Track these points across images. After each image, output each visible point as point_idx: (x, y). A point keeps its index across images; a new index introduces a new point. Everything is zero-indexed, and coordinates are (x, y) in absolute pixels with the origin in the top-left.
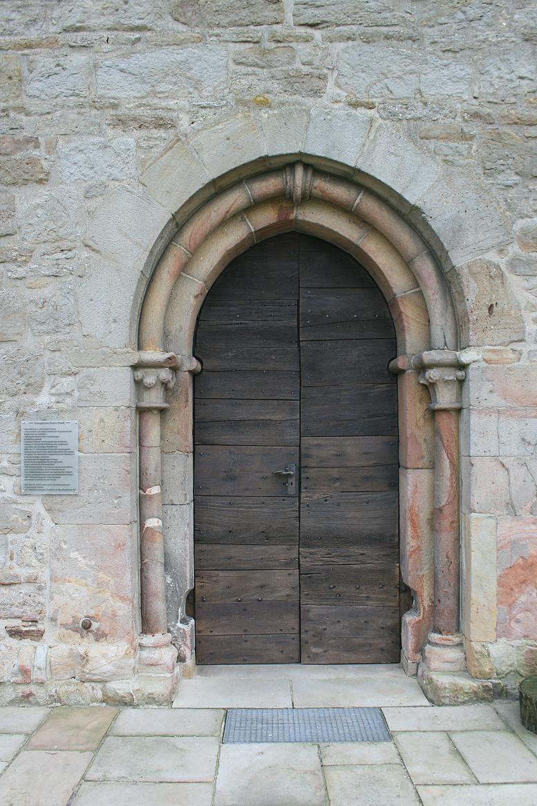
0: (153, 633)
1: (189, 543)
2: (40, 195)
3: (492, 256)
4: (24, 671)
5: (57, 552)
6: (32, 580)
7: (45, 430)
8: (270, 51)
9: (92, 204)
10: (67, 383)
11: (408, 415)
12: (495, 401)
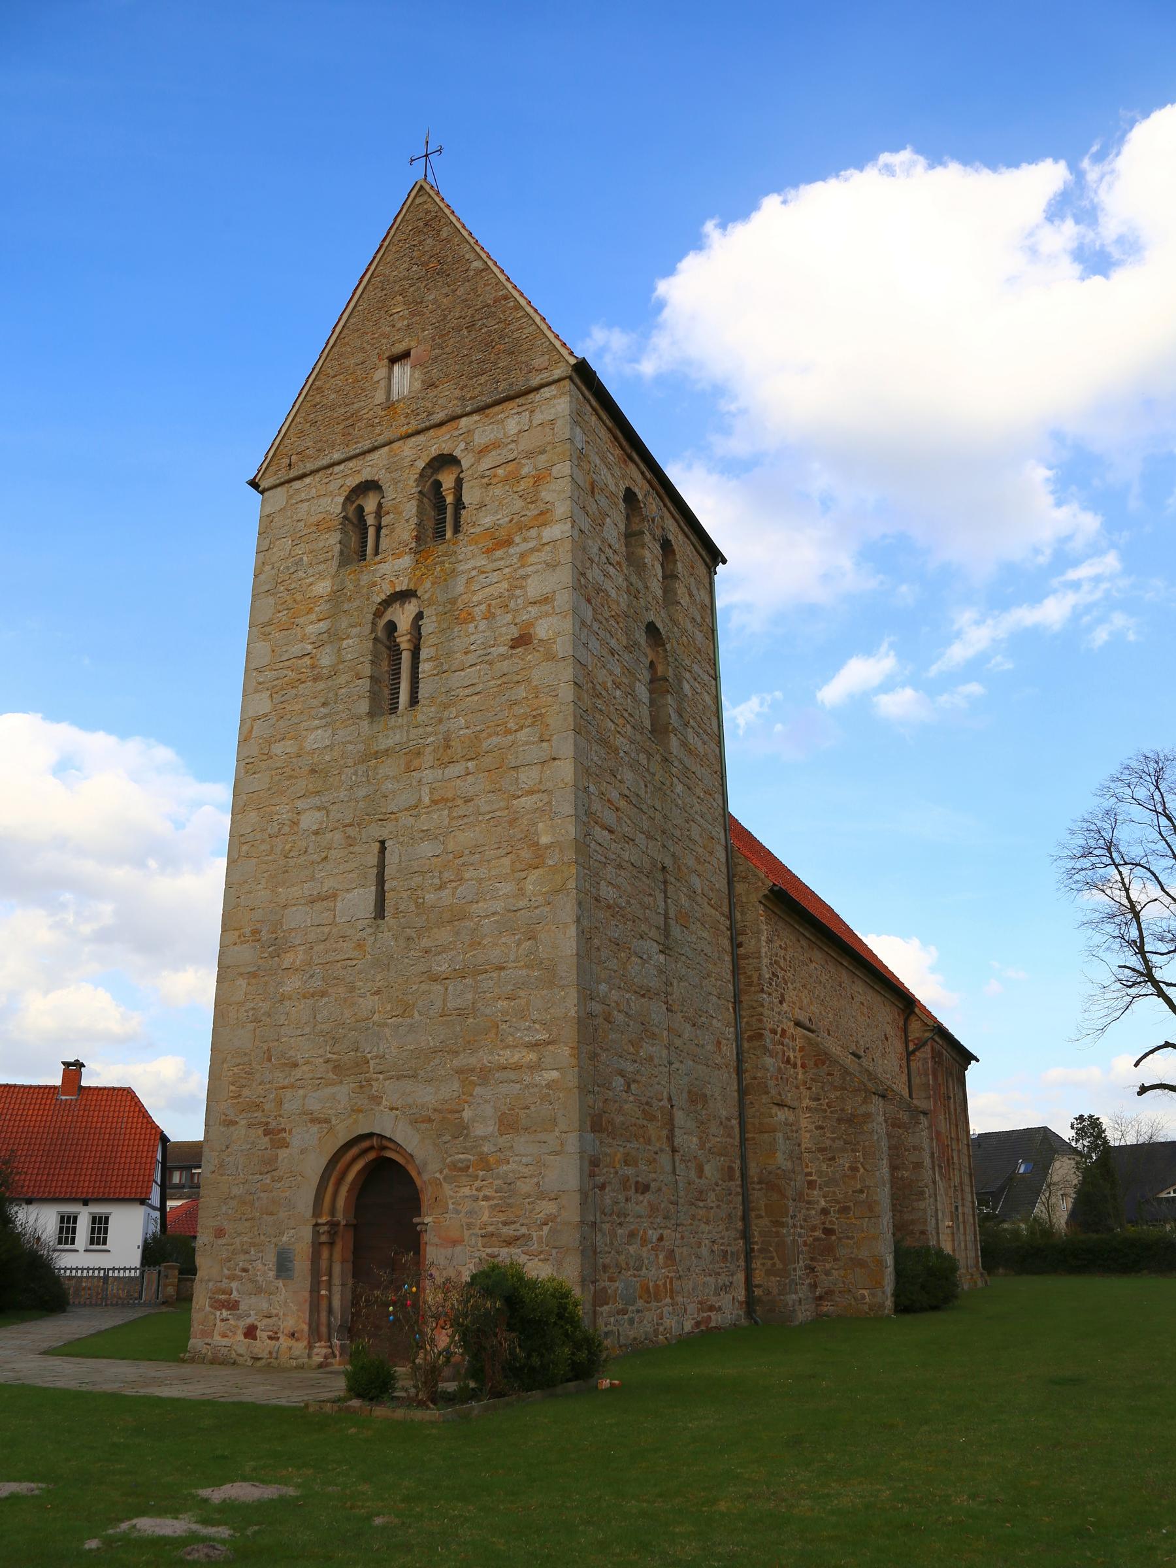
2: (287, 1151)
3: (437, 1175)
6: (277, 1315)
11: (428, 1249)
12: (436, 1240)
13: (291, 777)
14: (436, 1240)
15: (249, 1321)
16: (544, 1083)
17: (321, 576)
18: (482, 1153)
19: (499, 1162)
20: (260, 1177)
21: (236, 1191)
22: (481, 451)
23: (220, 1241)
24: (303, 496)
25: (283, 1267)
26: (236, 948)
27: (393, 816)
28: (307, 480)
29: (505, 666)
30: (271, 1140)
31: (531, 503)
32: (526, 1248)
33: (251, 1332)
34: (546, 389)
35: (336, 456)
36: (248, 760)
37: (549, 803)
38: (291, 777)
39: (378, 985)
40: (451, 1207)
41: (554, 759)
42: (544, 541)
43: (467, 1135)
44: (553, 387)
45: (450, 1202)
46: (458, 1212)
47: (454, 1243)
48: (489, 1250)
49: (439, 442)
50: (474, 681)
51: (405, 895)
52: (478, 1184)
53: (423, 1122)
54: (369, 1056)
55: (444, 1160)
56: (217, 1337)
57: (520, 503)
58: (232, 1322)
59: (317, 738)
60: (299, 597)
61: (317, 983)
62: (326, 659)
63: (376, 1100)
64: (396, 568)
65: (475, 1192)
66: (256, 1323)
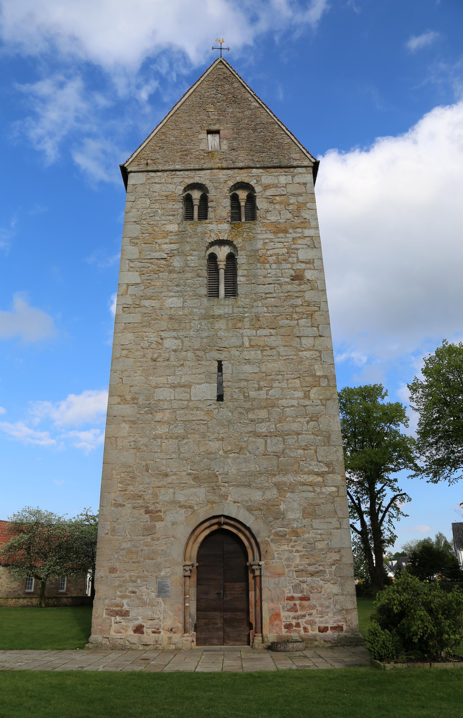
0: (187, 633)
1: (195, 610)
3: (267, 539)
4: (156, 641)
5: (165, 612)
6: (158, 619)
7: (162, 582)
8: (216, 489)
9: (174, 527)
10: (168, 570)
13: (156, 319)
14: (268, 574)
15: (137, 623)
16: (328, 493)
17: (170, 222)
18: (293, 528)
19: (304, 532)
20: (143, 538)
21: (124, 545)
22: (266, 186)
23: (113, 575)
24: (157, 181)
25: (162, 591)
26: (120, 406)
27: (226, 349)
28: (159, 174)
29: (289, 287)
30: (150, 516)
31: (297, 216)
32: (322, 577)
33: (139, 630)
34: (300, 168)
35: (178, 167)
36: (124, 306)
37: (320, 356)
38: (156, 319)
39: (222, 435)
40: (276, 556)
41: (320, 336)
42: (305, 235)
43: (283, 518)
44: (304, 169)
45: (275, 553)
46: (280, 559)
47: (280, 575)
48: (301, 579)
49: (242, 176)
50: (271, 291)
51: (237, 390)
52: (292, 544)
53: (256, 510)
54: (218, 473)
55: (270, 531)
56: (112, 633)
57: (289, 216)
58: (123, 623)
59: (173, 302)
60: (156, 229)
61: (180, 431)
62: (177, 263)
63: (225, 497)
64: (219, 228)
65: (290, 548)
66: (143, 624)
